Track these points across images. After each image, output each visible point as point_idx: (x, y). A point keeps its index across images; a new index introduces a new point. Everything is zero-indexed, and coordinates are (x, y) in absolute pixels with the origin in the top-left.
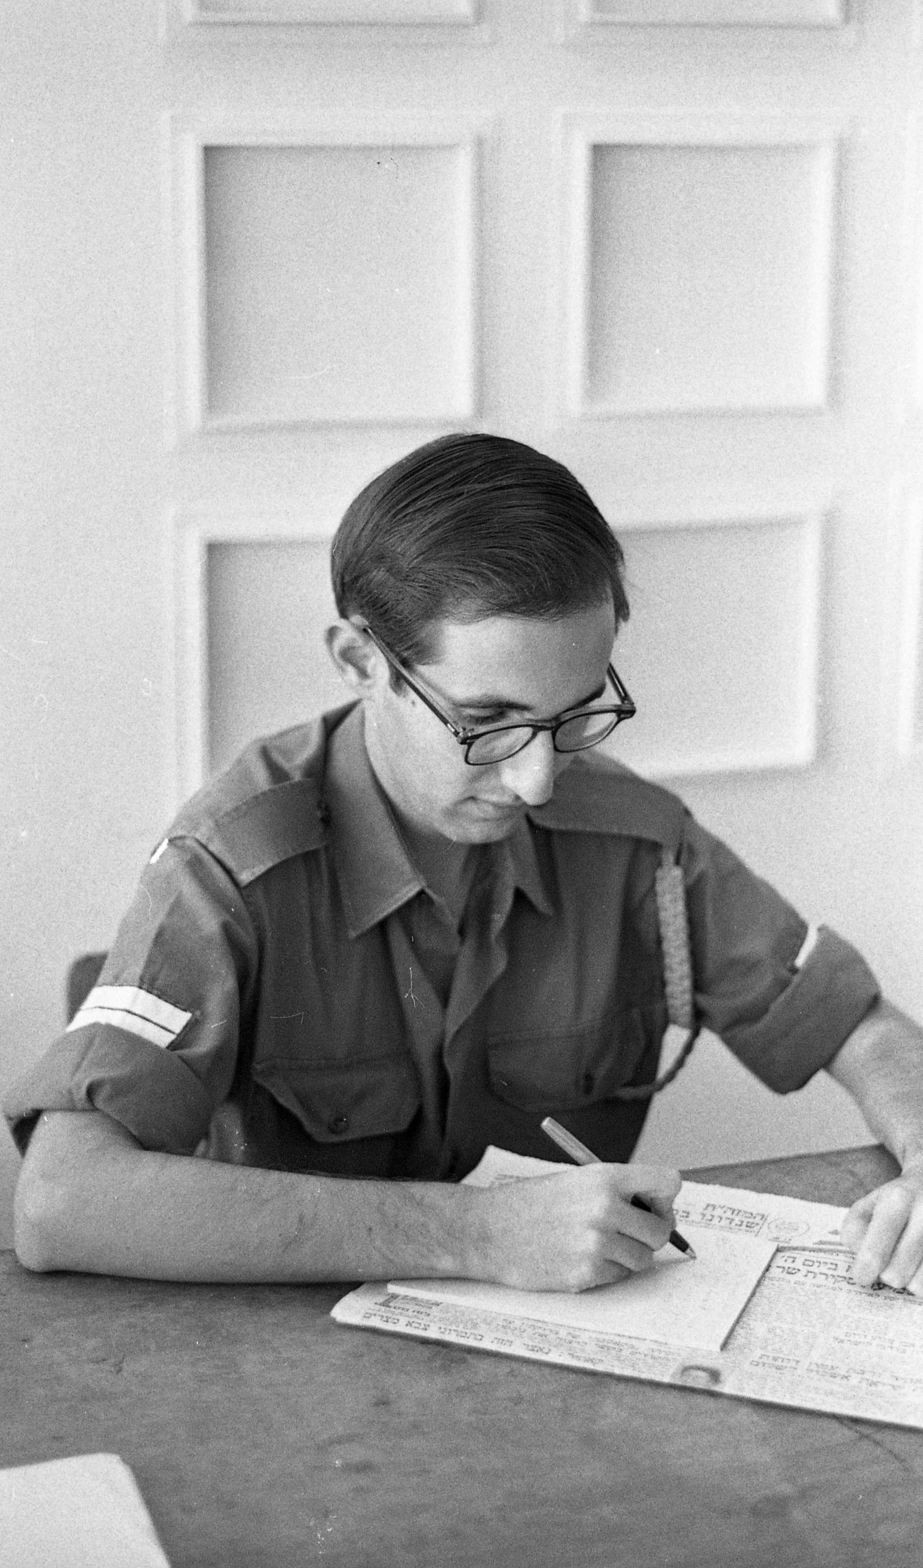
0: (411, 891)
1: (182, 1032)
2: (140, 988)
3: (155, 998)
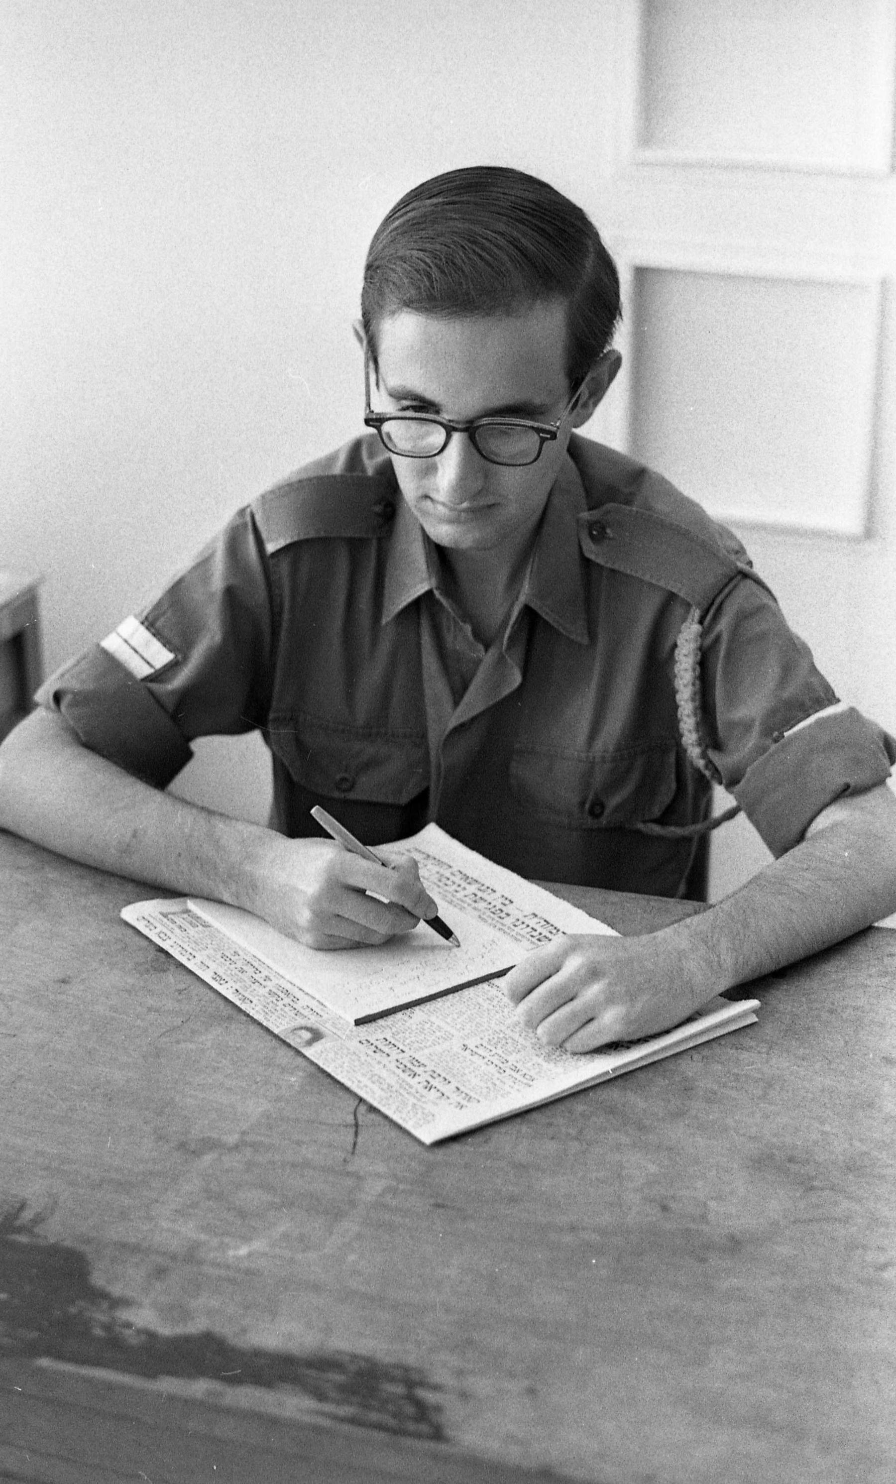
0: (421, 589)
1: (160, 670)
2: (142, 623)
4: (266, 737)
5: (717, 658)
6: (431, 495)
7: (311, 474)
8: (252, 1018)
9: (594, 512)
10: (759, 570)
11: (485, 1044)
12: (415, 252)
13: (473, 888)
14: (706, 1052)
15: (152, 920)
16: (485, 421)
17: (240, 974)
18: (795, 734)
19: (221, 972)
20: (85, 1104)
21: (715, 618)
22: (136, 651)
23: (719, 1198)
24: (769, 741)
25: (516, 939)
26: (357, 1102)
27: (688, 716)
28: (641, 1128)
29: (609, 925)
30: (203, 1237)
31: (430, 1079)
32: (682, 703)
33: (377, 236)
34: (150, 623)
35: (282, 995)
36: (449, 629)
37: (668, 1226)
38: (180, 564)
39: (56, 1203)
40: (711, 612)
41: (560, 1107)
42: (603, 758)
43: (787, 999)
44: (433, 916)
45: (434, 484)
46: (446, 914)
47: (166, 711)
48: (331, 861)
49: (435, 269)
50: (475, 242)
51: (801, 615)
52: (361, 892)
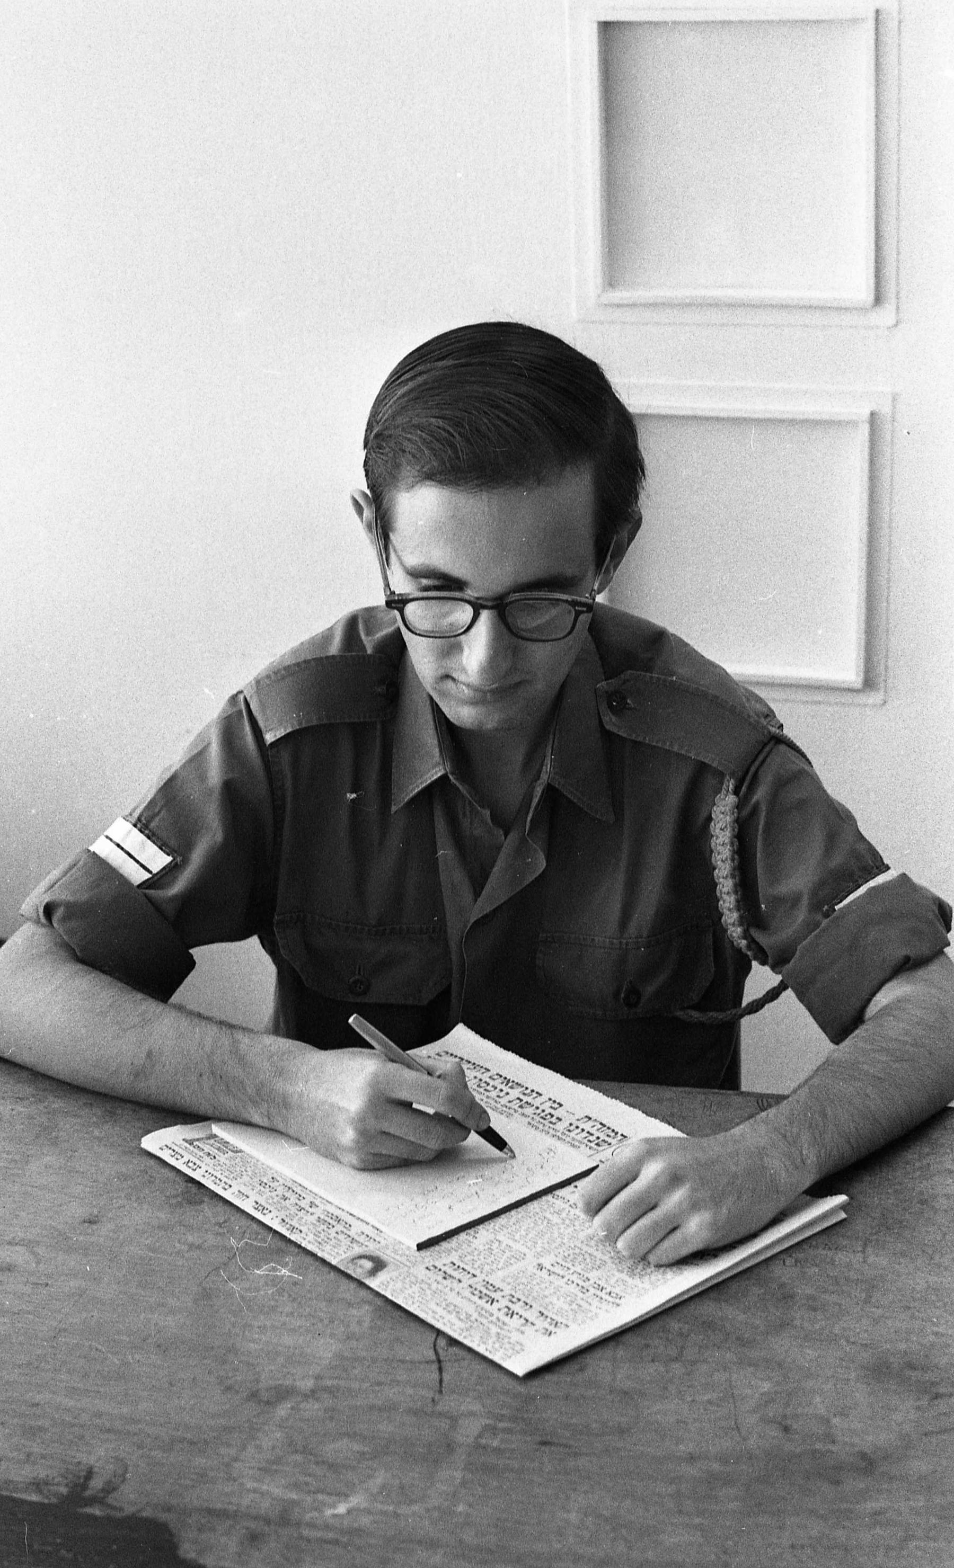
0: (437, 773)
1: (158, 873)
2: (135, 826)
3: (145, 838)
5: (757, 830)
6: (454, 675)
8: (304, 1249)
10: (789, 732)
11: (561, 1262)
12: (433, 420)
13: (515, 1093)
15: (176, 1149)
17: (282, 1201)
21: (752, 788)
23: (843, 1414)
24: (819, 917)
25: (573, 1146)
28: (743, 1342)
29: (669, 1124)
31: (510, 1305)
32: (721, 880)
33: (380, 401)
34: (144, 825)
36: (464, 814)
37: (788, 1447)
43: (878, 1193)
44: (485, 1127)
45: (456, 664)
46: (498, 1123)
47: (166, 918)
48: (376, 1075)
50: (497, 407)
51: (837, 779)
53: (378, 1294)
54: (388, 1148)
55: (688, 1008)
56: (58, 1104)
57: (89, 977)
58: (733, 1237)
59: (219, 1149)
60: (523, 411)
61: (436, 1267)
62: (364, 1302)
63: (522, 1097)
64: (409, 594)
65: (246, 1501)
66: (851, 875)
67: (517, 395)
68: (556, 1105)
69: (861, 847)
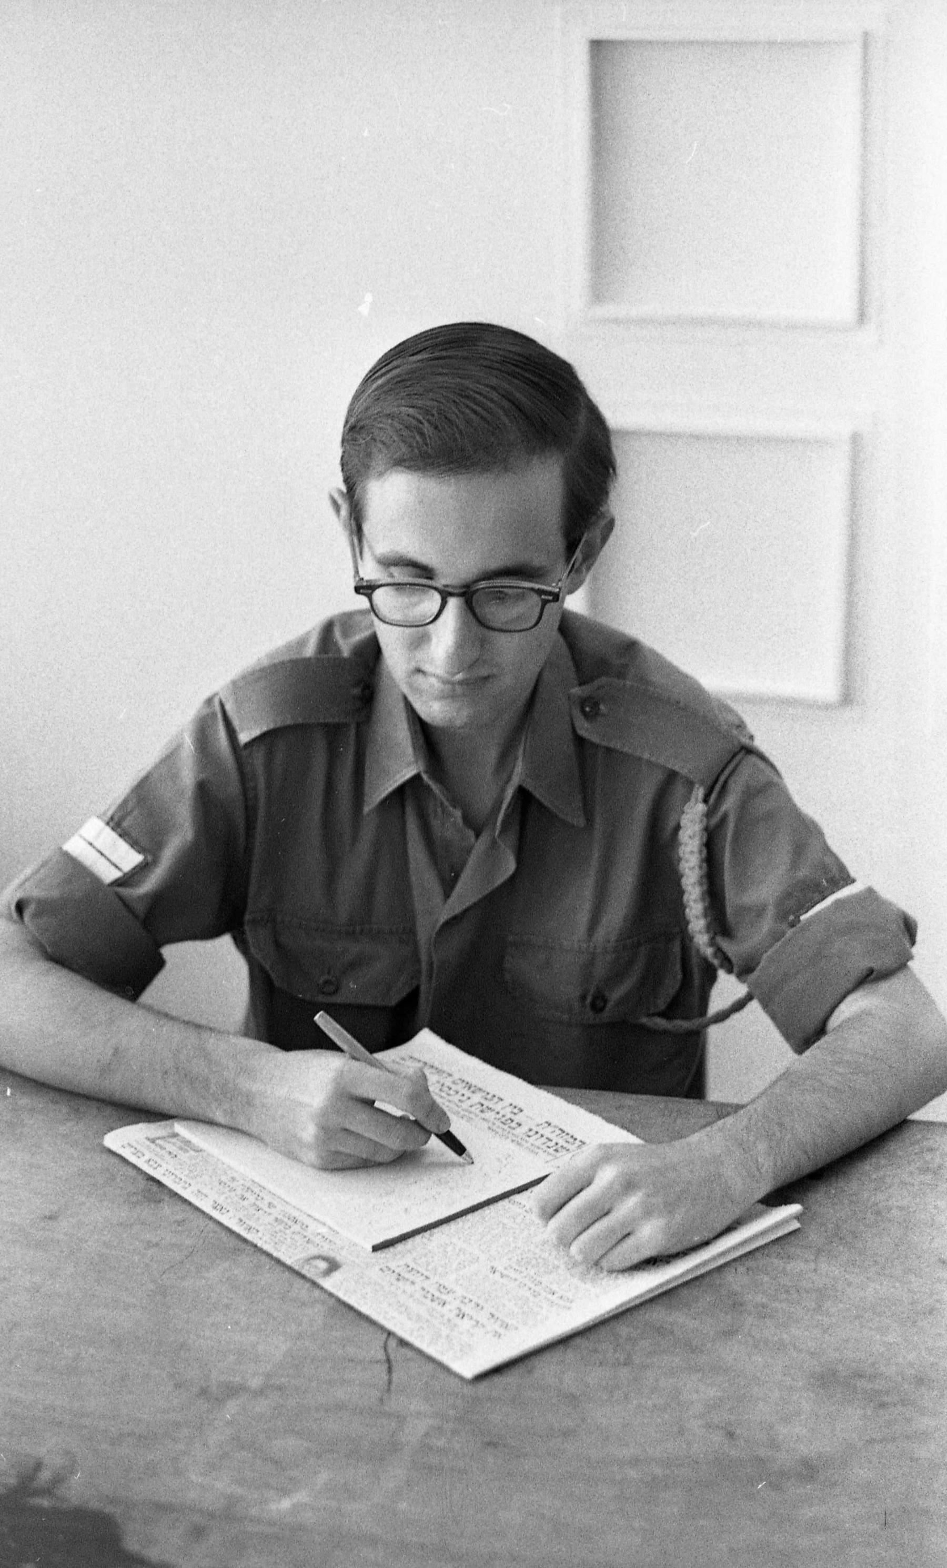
0: (408, 773)
1: (127, 874)
2: (108, 824)
4: (242, 944)
7: (286, 658)
9: (584, 687)
10: (761, 743)
13: (477, 1098)
14: (751, 1263)
15: (139, 1147)
16: (483, 584)
18: (812, 917)
19: (221, 1200)
20: (92, 1351)
22: (102, 854)
24: (784, 926)
26: (385, 1335)
27: (695, 901)
30: (239, 1491)
33: (356, 398)
34: (116, 823)
35: (290, 1223)
38: (143, 761)
39: (75, 1461)
40: (715, 789)
41: (603, 1332)
42: (605, 948)
43: (830, 1202)
44: (445, 1131)
45: (425, 659)
46: (458, 1129)
47: (136, 917)
49: (426, 424)
50: (467, 397)
51: (806, 790)
52: (370, 1103)
53: (331, 1295)
54: (350, 1147)
55: (653, 1015)
56: (24, 1101)
57: (60, 974)
58: (686, 1245)
59: (181, 1149)
60: (492, 400)
61: (389, 1269)
62: (316, 1301)
63: (483, 1101)
64: (376, 580)
65: (192, 1495)
66: (818, 885)
67: (487, 386)
68: (516, 1111)
69: (828, 860)
